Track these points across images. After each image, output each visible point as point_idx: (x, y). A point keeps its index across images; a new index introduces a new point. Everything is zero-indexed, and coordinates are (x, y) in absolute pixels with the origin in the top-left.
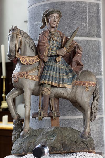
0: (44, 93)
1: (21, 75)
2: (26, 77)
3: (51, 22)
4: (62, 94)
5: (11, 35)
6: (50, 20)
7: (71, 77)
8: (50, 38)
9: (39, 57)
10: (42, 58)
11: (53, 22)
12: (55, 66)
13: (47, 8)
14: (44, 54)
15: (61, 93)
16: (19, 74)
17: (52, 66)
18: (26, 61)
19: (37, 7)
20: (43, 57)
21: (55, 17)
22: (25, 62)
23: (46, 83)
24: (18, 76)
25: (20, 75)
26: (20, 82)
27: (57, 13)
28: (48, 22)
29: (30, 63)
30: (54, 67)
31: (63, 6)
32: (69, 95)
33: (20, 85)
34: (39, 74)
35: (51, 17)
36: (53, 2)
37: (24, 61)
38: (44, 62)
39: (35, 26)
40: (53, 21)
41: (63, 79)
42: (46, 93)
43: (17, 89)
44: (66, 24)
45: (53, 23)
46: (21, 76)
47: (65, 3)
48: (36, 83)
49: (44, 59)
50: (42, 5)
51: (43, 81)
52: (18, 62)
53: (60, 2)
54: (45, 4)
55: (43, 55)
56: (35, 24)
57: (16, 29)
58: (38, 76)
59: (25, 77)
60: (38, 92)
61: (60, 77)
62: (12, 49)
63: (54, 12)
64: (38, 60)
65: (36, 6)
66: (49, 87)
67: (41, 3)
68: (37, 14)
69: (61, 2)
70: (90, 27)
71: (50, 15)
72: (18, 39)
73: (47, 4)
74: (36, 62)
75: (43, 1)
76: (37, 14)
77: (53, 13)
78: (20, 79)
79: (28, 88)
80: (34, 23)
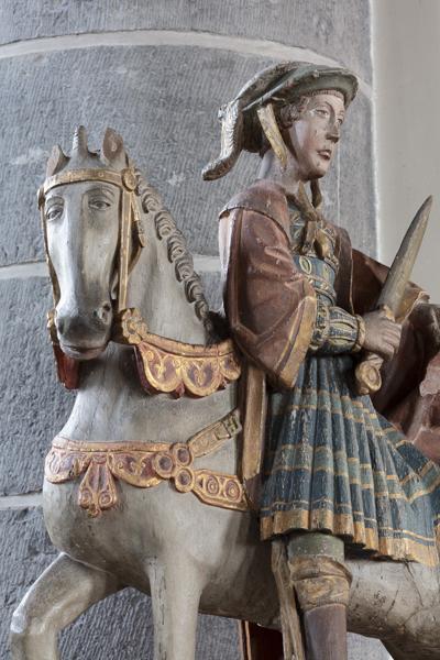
0: (321, 593)
1: (149, 463)
2: (177, 483)
3: (308, 141)
4: (385, 607)
5: (86, 186)
6: (299, 130)
7: (423, 496)
8: (302, 241)
9: (244, 356)
10: (267, 359)
11: (324, 144)
12: (351, 417)
13: (122, 71)
14: (287, 339)
15: (383, 600)
16: (129, 460)
17: (320, 414)
18: (170, 370)
19: (45, 61)
20: (277, 352)
21: (332, 110)
22: (166, 376)
23: (329, 525)
24: (122, 472)
25: (139, 467)
26: (130, 513)
27: (339, 90)
28: (287, 139)
29: (193, 389)
30: (346, 421)
31: (223, 73)
32: (425, 612)
33: (123, 535)
34: (252, 465)
35: (312, 112)
36: (165, 43)
37: (161, 369)
38: (274, 385)
39: (20, 174)
40: (322, 133)
41: (393, 501)
42: (333, 597)
43: (81, 565)
44: (237, 184)
45: (321, 147)
46: (149, 472)
47: (232, 63)
48: (231, 522)
49: (281, 366)
50: (84, 52)
51: (306, 512)
52: (90, 379)
53: (207, 49)
54: (111, 50)
55: (277, 344)
56: (20, 161)
57: (117, 151)
58: (246, 476)
59: (172, 480)
60: (233, 585)
61: (382, 491)
62: (98, 283)
63: (328, 85)
64: (234, 370)
65: (40, 57)
66: (337, 549)
67: (80, 38)
68: (45, 101)
69: (216, 50)
70: (347, 218)
71: (308, 94)
72: (127, 219)
73: (121, 48)
74: (221, 388)
75: (93, 32)
76: (45, 101)
77: (328, 85)
78: (139, 492)
79: (189, 556)
80: (16, 155)
